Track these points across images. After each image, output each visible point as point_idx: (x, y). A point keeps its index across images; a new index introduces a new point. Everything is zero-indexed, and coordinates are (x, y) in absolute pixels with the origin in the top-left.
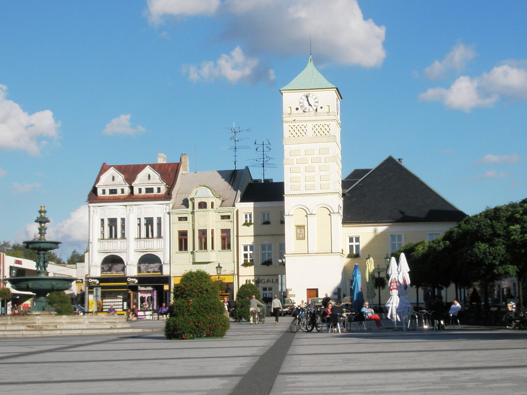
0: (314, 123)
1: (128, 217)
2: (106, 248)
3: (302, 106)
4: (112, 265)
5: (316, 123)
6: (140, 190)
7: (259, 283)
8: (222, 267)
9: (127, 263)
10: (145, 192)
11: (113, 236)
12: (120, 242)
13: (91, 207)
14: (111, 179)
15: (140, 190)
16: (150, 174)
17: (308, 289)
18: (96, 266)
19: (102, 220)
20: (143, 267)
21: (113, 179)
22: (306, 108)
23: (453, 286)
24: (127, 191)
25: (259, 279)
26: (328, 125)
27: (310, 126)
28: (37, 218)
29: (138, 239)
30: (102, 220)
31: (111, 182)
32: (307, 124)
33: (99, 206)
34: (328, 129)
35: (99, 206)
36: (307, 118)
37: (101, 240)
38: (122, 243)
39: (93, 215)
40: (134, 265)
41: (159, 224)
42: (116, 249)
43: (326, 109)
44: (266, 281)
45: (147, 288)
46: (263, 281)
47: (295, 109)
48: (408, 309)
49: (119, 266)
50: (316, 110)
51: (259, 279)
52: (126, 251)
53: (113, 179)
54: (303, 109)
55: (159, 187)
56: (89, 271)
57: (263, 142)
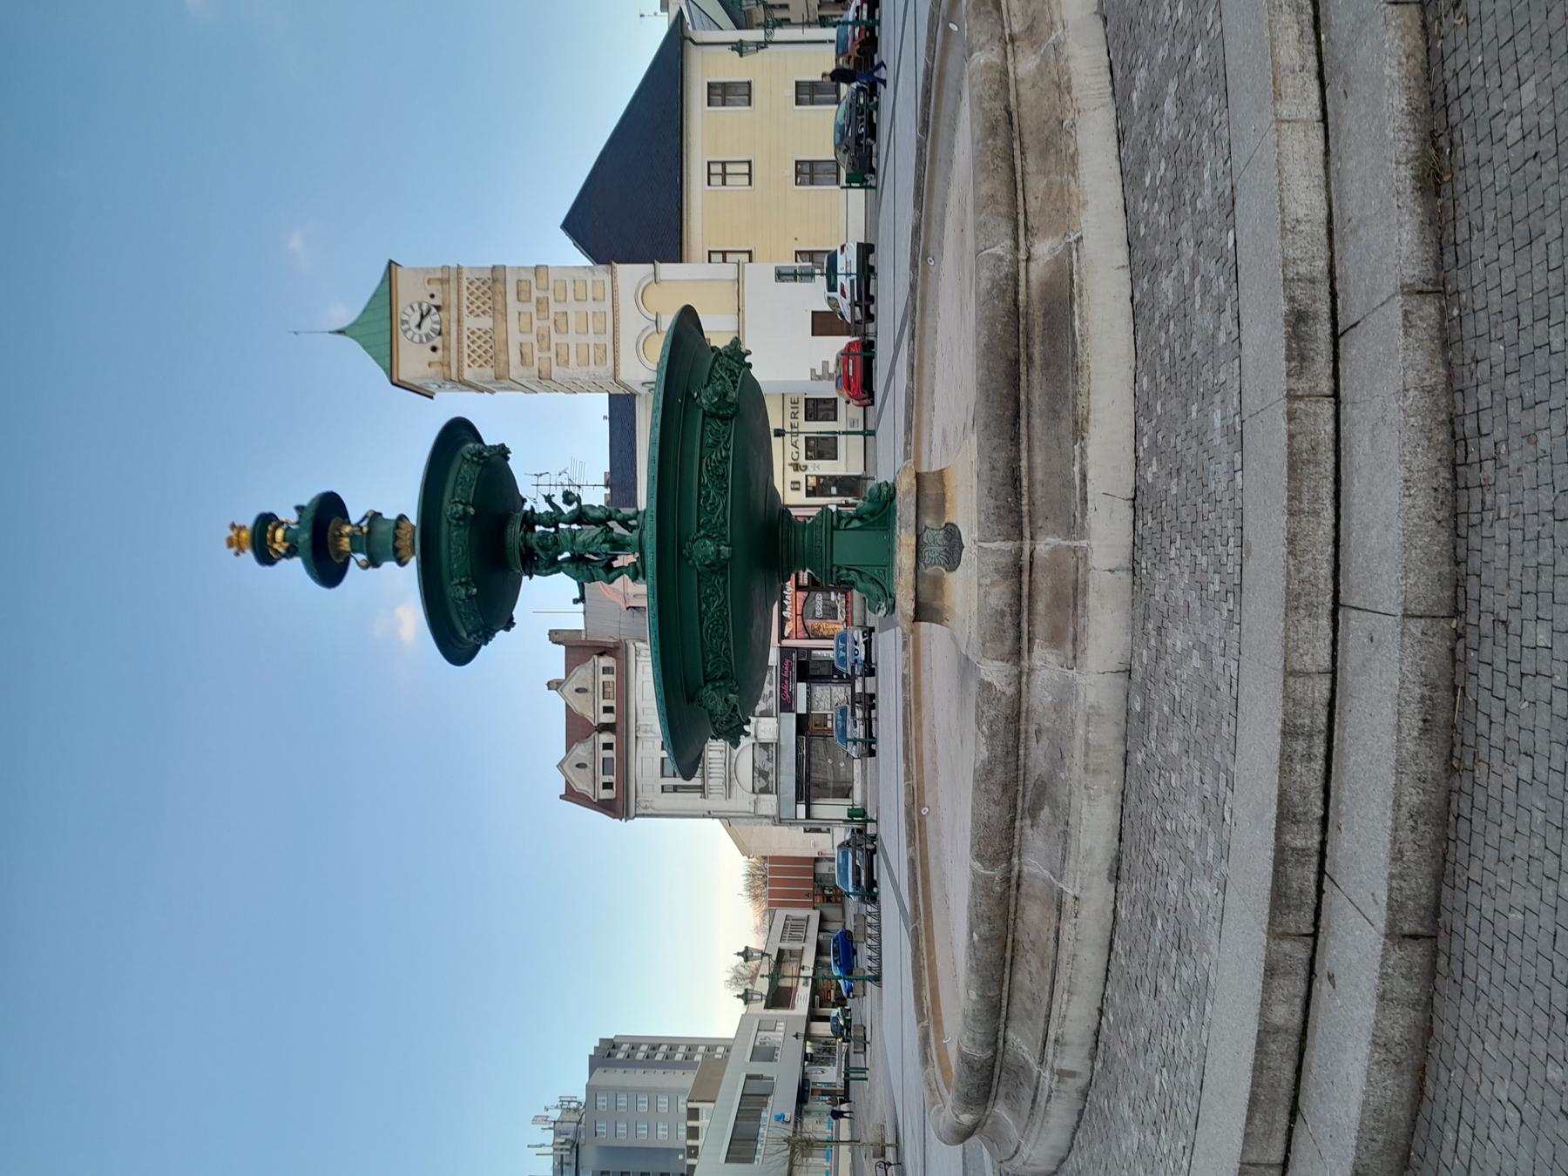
0: (465, 312)
3: (428, 338)
5: (464, 309)
6: (607, 786)
7: (797, 465)
8: (747, 948)
13: (638, 812)
14: (582, 770)
15: (607, 786)
16: (575, 687)
17: (813, 334)
22: (433, 330)
24: (606, 738)
25: (790, 465)
26: (470, 283)
27: (470, 322)
31: (588, 771)
32: (465, 329)
34: (478, 283)
36: (454, 327)
37: (704, 792)
39: (654, 809)
43: (435, 288)
44: (795, 449)
45: (813, 512)
46: (795, 456)
47: (433, 354)
50: (438, 308)
51: (790, 465)
54: (433, 335)
56: (766, 817)
57: (529, 1146)
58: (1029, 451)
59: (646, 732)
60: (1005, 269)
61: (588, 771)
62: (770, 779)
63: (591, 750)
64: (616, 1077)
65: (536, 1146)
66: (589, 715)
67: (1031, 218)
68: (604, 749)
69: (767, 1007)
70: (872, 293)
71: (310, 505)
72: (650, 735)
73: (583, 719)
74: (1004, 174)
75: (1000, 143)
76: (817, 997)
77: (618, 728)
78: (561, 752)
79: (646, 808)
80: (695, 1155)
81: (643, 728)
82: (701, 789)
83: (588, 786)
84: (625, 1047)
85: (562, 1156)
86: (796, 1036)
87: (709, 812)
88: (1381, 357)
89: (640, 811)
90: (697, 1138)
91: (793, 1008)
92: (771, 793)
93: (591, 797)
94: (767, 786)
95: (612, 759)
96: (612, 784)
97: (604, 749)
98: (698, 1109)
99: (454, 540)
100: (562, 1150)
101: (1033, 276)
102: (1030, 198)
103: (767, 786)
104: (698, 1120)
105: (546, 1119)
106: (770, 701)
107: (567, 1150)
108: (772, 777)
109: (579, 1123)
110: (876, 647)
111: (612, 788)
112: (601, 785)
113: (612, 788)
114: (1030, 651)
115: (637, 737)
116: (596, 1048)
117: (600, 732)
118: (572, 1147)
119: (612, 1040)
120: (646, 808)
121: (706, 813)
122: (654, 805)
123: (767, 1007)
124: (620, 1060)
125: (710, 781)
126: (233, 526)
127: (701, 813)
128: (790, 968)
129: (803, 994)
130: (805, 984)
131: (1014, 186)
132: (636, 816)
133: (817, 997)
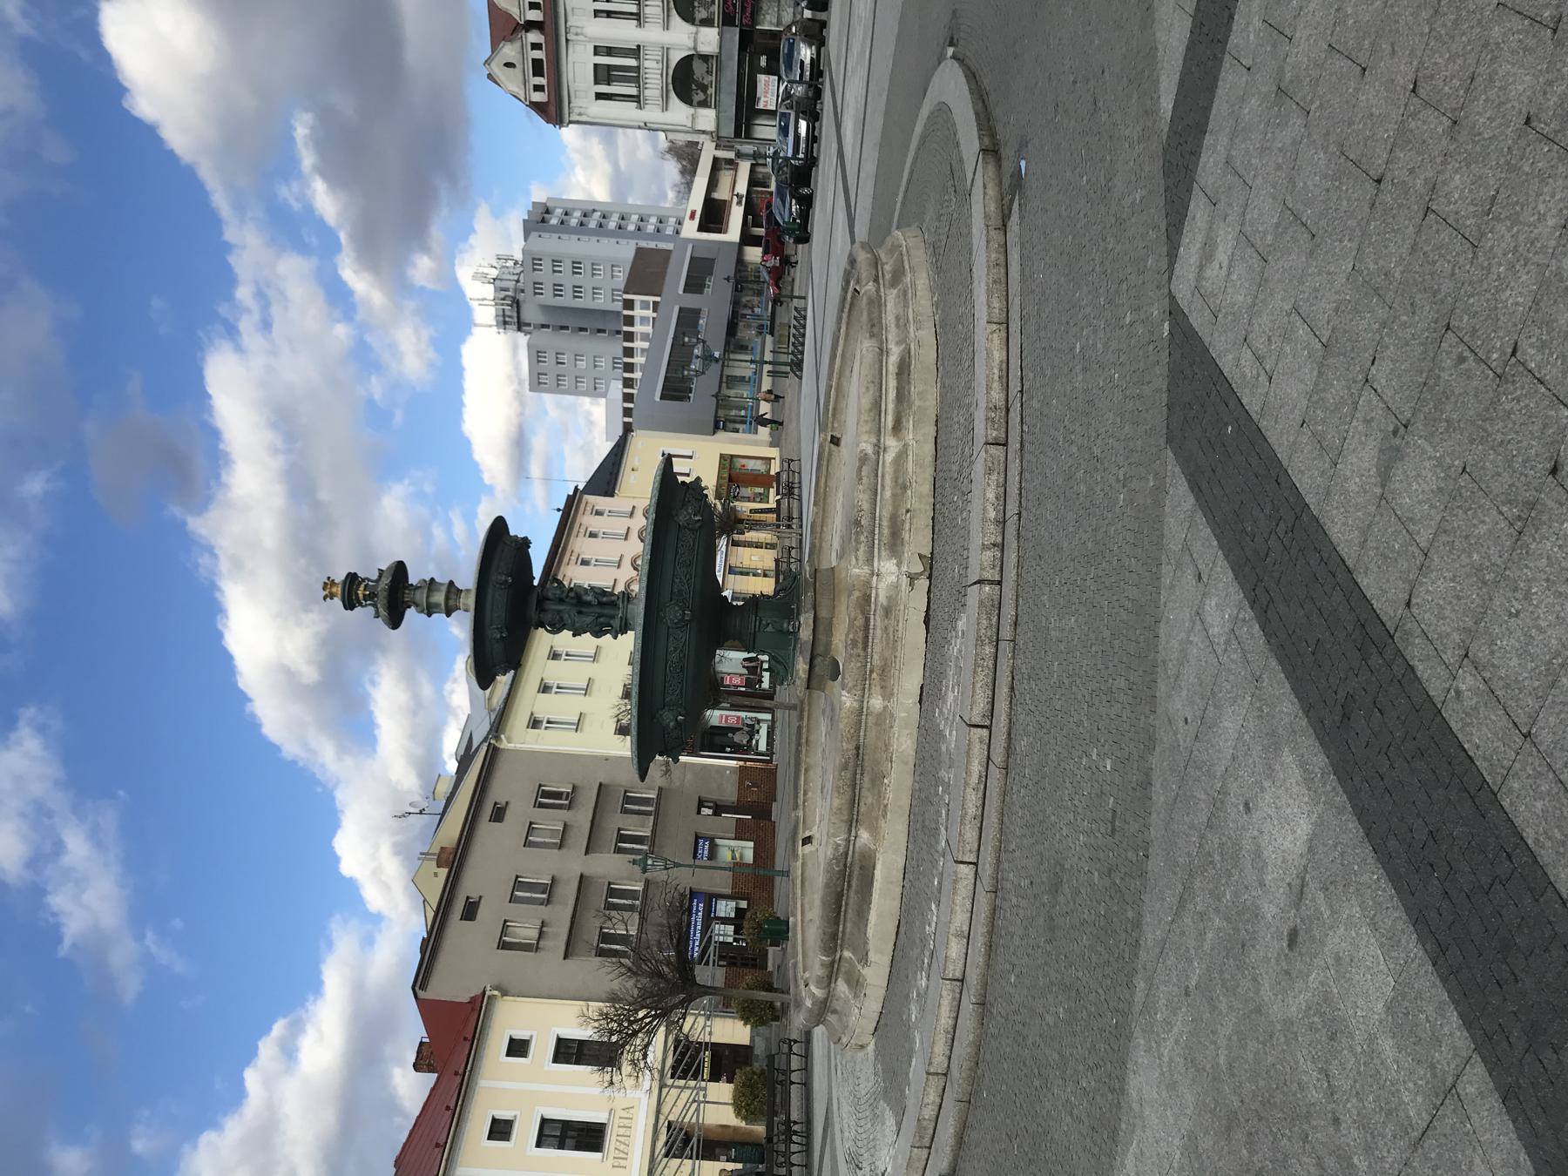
1: (591, 40)
2: (658, 93)
4: (694, 81)
6: (538, 88)
9: (690, 49)
10: (540, 52)
11: (635, 76)
12: (646, 62)
14: (510, 70)
15: (538, 88)
18: (694, 117)
19: (599, 96)
20: (701, 14)
21: (509, 65)
23: (724, 594)
24: (534, 37)
28: (615, 638)
29: (639, 20)
30: (597, 13)
31: (517, 71)
33: (569, 103)
35: (569, 103)
38: (647, 57)
40: (696, 33)
41: (610, 51)
42: (660, 72)
48: (733, 851)
49: (699, 68)
52: (666, 51)
53: (509, 65)
55: (530, 62)
56: (704, 132)
58: (845, 921)
59: (577, 34)
60: (841, 849)
61: (517, 71)
62: (709, 92)
63: (519, 49)
64: (550, 244)
65: (478, 300)
66: (515, 12)
67: (860, 817)
68: (532, 49)
69: (701, 228)
70: (816, 134)
71: (388, 569)
72: (581, 38)
73: (509, 16)
74: (848, 796)
75: (849, 775)
76: (750, 217)
77: (548, 26)
78: (486, 50)
79: (580, 114)
80: (632, 324)
81: (573, 30)
82: (636, 99)
83: (518, 87)
84: (559, 211)
85: (504, 310)
86: (728, 279)
87: (645, 124)
88: (1040, 848)
89: (574, 118)
90: (632, 309)
91: (725, 232)
92: (710, 107)
93: (518, 19)
94: (706, 100)
95: (542, 60)
96: (541, 44)
97: (532, 49)
98: (633, 301)
99: (498, 600)
100: (503, 304)
101: (857, 845)
102: (862, 804)
103: (706, 100)
104: (632, 357)
105: (485, 275)
106: (711, 9)
107: (508, 305)
108: (711, 91)
109: (518, 281)
110: (812, 224)
111: (543, 91)
112: (532, 87)
113: (543, 91)
114: (836, 980)
115: (567, 40)
116: (529, 212)
117: (527, 31)
118: (513, 302)
119: (545, 204)
120: (580, 114)
121: (643, 125)
122: (585, 30)
123: (701, 228)
124: (553, 226)
125: (646, 91)
126: (329, 578)
127: (637, 124)
128: (725, 178)
129: (736, 215)
130: (739, 203)
131: (854, 802)
132: (570, 122)
133: (750, 217)
